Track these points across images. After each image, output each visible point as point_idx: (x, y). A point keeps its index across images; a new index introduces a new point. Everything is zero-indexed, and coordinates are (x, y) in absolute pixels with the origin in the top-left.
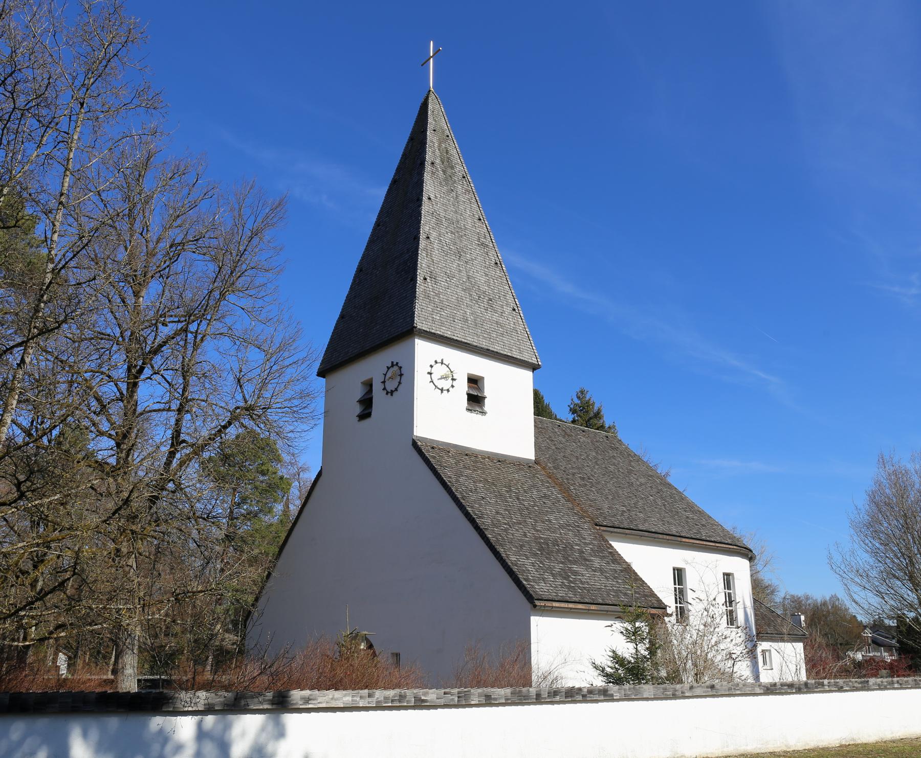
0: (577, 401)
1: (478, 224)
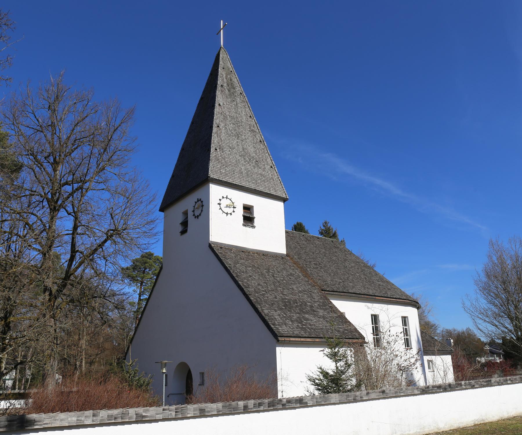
0: (323, 228)
1: (250, 119)
